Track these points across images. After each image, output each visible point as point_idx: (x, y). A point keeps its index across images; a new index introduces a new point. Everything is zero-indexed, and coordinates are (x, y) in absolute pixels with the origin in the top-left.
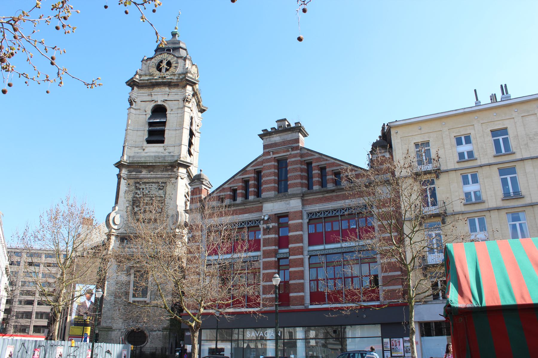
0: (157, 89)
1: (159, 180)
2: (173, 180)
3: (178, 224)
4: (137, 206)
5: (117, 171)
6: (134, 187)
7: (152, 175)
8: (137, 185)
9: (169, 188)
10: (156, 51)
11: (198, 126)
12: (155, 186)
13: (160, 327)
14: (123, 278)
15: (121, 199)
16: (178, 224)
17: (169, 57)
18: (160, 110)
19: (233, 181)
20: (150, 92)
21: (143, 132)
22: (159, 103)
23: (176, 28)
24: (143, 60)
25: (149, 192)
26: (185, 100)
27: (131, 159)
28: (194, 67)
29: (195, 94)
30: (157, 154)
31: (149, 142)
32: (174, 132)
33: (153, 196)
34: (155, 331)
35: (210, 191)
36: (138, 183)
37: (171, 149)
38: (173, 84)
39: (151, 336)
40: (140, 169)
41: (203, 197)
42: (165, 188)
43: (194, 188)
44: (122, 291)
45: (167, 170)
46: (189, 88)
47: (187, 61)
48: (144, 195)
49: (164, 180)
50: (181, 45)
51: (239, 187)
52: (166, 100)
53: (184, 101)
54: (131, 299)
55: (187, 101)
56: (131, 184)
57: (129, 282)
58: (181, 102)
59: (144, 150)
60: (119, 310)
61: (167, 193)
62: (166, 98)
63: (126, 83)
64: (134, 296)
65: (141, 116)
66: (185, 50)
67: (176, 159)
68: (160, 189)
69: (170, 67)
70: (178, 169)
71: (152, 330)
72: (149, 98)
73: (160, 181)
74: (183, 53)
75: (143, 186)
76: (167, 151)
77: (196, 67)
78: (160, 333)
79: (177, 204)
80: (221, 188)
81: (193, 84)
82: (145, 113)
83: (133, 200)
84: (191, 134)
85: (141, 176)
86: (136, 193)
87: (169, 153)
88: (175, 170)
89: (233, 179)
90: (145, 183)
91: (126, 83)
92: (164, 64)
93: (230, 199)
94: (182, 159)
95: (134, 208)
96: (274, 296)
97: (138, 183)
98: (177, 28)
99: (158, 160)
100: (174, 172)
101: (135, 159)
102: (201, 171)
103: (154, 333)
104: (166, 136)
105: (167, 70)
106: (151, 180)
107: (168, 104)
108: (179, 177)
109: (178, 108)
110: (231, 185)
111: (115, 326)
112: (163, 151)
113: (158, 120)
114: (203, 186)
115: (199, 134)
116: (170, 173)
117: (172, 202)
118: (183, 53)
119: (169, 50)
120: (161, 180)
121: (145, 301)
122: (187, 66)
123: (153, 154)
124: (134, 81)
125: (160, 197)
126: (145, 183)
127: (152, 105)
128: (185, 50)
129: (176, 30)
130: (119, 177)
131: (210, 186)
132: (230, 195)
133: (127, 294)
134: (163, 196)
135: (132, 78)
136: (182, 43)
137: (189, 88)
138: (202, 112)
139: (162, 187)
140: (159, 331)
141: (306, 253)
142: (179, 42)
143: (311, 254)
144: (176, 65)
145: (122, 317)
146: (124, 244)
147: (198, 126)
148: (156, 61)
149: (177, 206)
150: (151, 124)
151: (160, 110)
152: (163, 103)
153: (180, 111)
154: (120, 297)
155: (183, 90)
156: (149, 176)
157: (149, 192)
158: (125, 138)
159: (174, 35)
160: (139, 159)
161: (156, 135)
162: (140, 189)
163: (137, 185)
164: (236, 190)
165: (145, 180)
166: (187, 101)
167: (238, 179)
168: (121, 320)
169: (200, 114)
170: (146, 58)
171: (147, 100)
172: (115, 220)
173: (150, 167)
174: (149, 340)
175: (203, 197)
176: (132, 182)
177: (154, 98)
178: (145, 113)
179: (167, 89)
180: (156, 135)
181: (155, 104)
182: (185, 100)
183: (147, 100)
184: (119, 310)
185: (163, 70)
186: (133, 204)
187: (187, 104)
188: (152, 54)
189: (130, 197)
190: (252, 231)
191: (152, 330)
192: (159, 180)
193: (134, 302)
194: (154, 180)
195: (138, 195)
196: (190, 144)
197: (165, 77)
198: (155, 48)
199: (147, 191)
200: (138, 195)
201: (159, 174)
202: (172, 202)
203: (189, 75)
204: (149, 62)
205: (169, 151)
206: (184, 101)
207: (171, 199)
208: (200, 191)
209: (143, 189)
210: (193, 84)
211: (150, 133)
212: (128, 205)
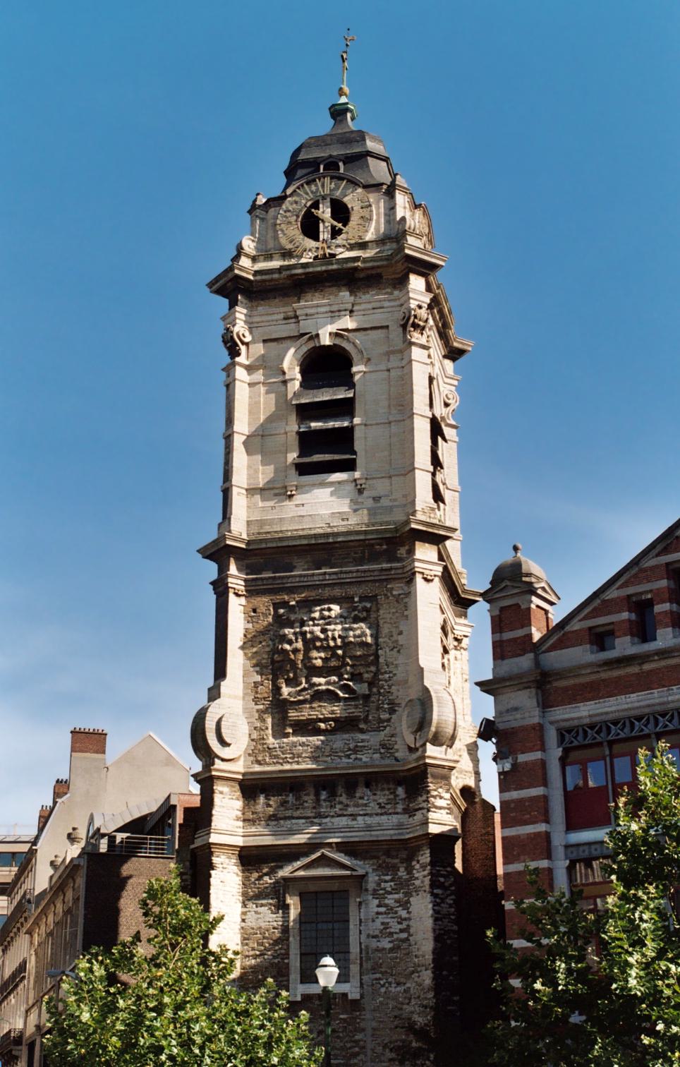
1: (351, 591)
2: (398, 588)
3: (433, 729)
5: (211, 569)
10: (290, 174)
11: (447, 405)
14: (266, 917)
15: (236, 660)
16: (433, 729)
17: (337, 188)
19: (635, 576)
23: (341, 92)
24: (253, 208)
26: (408, 323)
27: (255, 529)
28: (418, 213)
29: (435, 303)
35: (557, 615)
38: (362, 275)
41: (537, 636)
42: (373, 615)
43: (502, 609)
45: (375, 557)
46: (416, 283)
47: (401, 199)
48: (305, 641)
50: (371, 145)
51: (657, 592)
53: (404, 327)
55: (415, 326)
56: (262, 609)
58: (396, 331)
61: (385, 630)
63: (210, 285)
66: (386, 159)
67: (399, 517)
69: (346, 221)
70: (411, 551)
72: (290, 329)
74: (378, 171)
76: (366, 493)
77: (425, 213)
79: (422, 663)
80: (596, 602)
81: (425, 269)
82: (281, 378)
83: (273, 662)
84: (436, 430)
88: (402, 551)
89: (635, 570)
91: (210, 285)
92: (325, 212)
93: (632, 635)
94: (420, 516)
98: (346, 90)
100: (400, 560)
101: (267, 528)
102: (516, 549)
104: (358, 446)
105: (335, 233)
108: (419, 578)
110: (631, 590)
114: (534, 598)
115: (454, 431)
116: (385, 566)
117: (401, 660)
118: (378, 171)
119: (331, 165)
120: (361, 590)
122: (400, 213)
124: (238, 277)
128: (386, 159)
129: (343, 100)
130: (221, 588)
131: (552, 598)
132: (629, 620)
135: (231, 269)
136: (374, 139)
137: (416, 283)
138: (454, 359)
141: (559, 852)
142: (361, 136)
143: (574, 856)
144: (365, 213)
147: (447, 405)
148: (299, 202)
149: (422, 669)
152: (338, 341)
153: (394, 362)
155: (396, 293)
159: (338, 113)
164: (650, 603)
166: (415, 326)
167: (652, 568)
169: (449, 365)
170: (262, 200)
172: (223, 731)
175: (537, 636)
176: (263, 602)
177: (306, 326)
179: (345, 295)
181: (311, 345)
182: (408, 323)
185: (324, 234)
187: (416, 337)
188: (276, 185)
190: (623, 755)
196: (436, 462)
197: (333, 256)
198: (285, 164)
200: (290, 642)
201: (352, 570)
202: (401, 660)
203: (411, 240)
204: (272, 211)
205: (374, 494)
206: (404, 327)
207: (397, 648)
208: (524, 618)
210: (425, 269)
211: (308, 442)
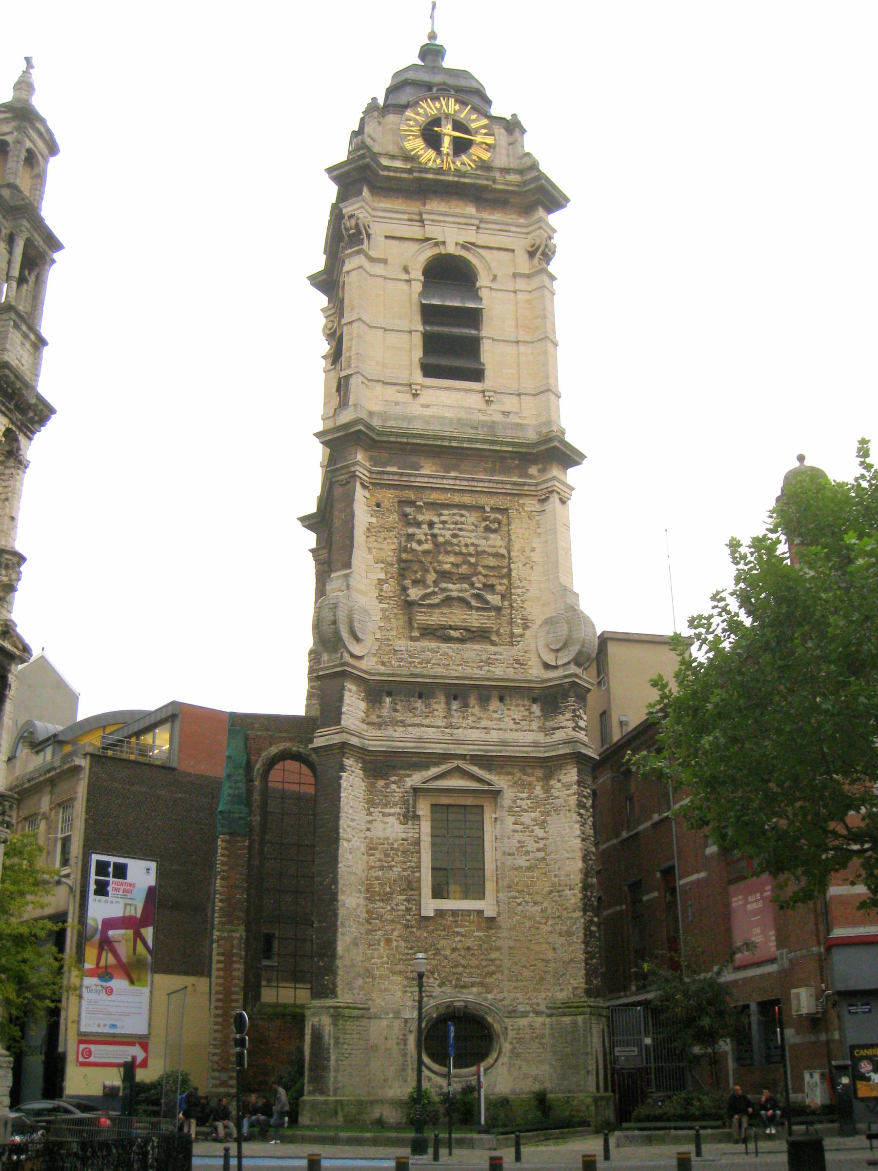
0: (435, 206)
1: (483, 500)
4: (415, 582)
6: (395, 516)
7: (453, 479)
8: (408, 510)
9: (519, 528)
12: (471, 518)
13: (541, 999)
18: (449, 273)
20: (416, 210)
21: (406, 336)
22: (451, 249)
25: (455, 536)
30: (463, 414)
31: (428, 371)
32: (511, 349)
33: (471, 549)
34: (525, 1015)
36: (412, 503)
37: (510, 403)
39: (511, 1034)
40: (413, 459)
44: (393, 874)
48: (437, 545)
49: (498, 501)
52: (473, 244)
54: (430, 906)
56: (386, 504)
57: (417, 842)
59: (415, 395)
60: (388, 941)
62: (470, 236)
64: (438, 893)
65: (391, 285)
68: (487, 529)
71: (513, 1013)
72: (416, 232)
73: (488, 502)
75: (427, 516)
76: (493, 407)
78: (539, 1020)
82: (405, 277)
83: (401, 561)
85: (419, 481)
86: (410, 537)
87: (506, 414)
90: (434, 506)
95: (404, 589)
96: (861, 889)
97: (412, 503)
99: (469, 433)
103: (523, 1022)
106: (457, 499)
107: (481, 257)
109: (515, 276)
111: (378, 1002)
112: (483, 406)
113: (457, 304)
121: (480, 912)
123: (449, 414)
125: (496, 555)
126: (434, 506)
127: (429, 253)
133: (412, 886)
134: (503, 551)
139: (496, 522)
140: (538, 1013)
145: (399, 967)
146: (385, 712)
150: (428, 313)
151: (449, 273)
154: (386, 898)
156: (446, 483)
157: (455, 536)
158: (336, 356)
160: (405, 425)
161: (451, 346)
162: (418, 525)
163: (408, 510)
165: (434, 497)
168: (398, 979)
171: (400, 242)
173: (448, 452)
174: (507, 1047)
176: (388, 497)
177: (432, 231)
178: (405, 277)
180: (451, 346)
181: (436, 251)
183: (400, 242)
184: (388, 941)
186: (402, 575)
189: (389, 548)
191: (513, 1013)
192: (483, 500)
193: (440, 913)
194: (467, 499)
195: (420, 542)
199: (448, 534)
200: (420, 542)
201: (482, 479)
209: (431, 525)
211: (431, 344)
212: (382, 576)
